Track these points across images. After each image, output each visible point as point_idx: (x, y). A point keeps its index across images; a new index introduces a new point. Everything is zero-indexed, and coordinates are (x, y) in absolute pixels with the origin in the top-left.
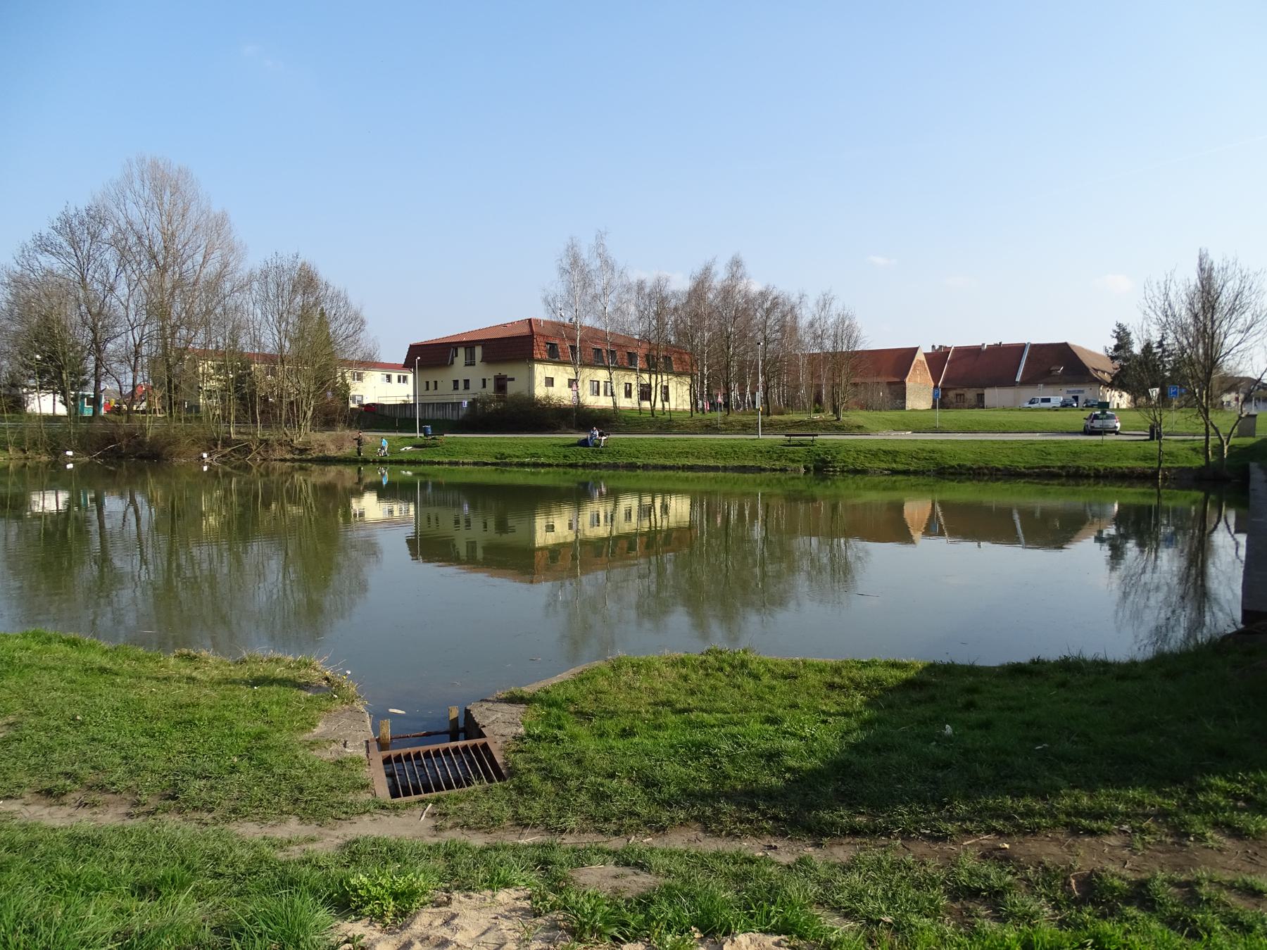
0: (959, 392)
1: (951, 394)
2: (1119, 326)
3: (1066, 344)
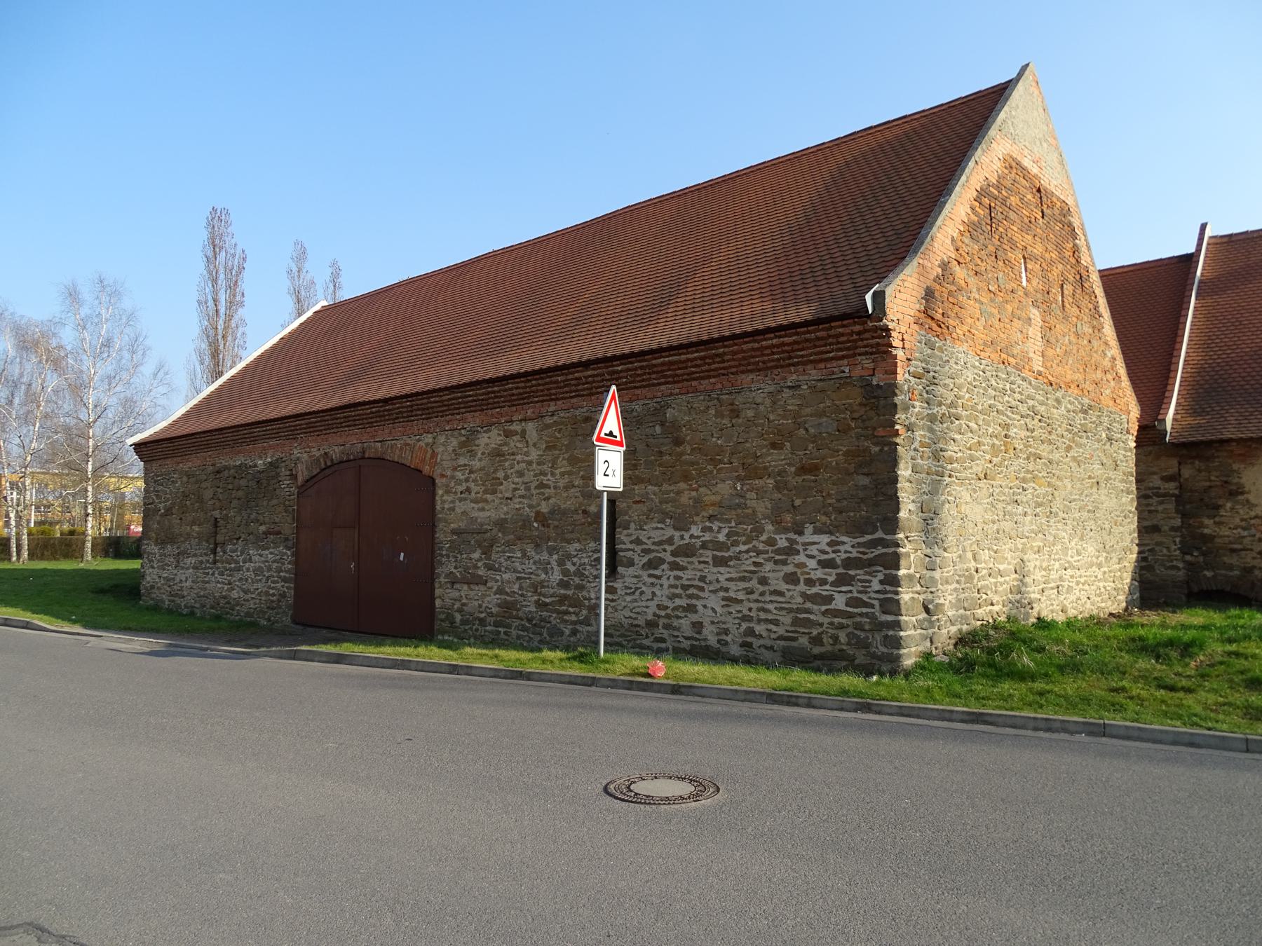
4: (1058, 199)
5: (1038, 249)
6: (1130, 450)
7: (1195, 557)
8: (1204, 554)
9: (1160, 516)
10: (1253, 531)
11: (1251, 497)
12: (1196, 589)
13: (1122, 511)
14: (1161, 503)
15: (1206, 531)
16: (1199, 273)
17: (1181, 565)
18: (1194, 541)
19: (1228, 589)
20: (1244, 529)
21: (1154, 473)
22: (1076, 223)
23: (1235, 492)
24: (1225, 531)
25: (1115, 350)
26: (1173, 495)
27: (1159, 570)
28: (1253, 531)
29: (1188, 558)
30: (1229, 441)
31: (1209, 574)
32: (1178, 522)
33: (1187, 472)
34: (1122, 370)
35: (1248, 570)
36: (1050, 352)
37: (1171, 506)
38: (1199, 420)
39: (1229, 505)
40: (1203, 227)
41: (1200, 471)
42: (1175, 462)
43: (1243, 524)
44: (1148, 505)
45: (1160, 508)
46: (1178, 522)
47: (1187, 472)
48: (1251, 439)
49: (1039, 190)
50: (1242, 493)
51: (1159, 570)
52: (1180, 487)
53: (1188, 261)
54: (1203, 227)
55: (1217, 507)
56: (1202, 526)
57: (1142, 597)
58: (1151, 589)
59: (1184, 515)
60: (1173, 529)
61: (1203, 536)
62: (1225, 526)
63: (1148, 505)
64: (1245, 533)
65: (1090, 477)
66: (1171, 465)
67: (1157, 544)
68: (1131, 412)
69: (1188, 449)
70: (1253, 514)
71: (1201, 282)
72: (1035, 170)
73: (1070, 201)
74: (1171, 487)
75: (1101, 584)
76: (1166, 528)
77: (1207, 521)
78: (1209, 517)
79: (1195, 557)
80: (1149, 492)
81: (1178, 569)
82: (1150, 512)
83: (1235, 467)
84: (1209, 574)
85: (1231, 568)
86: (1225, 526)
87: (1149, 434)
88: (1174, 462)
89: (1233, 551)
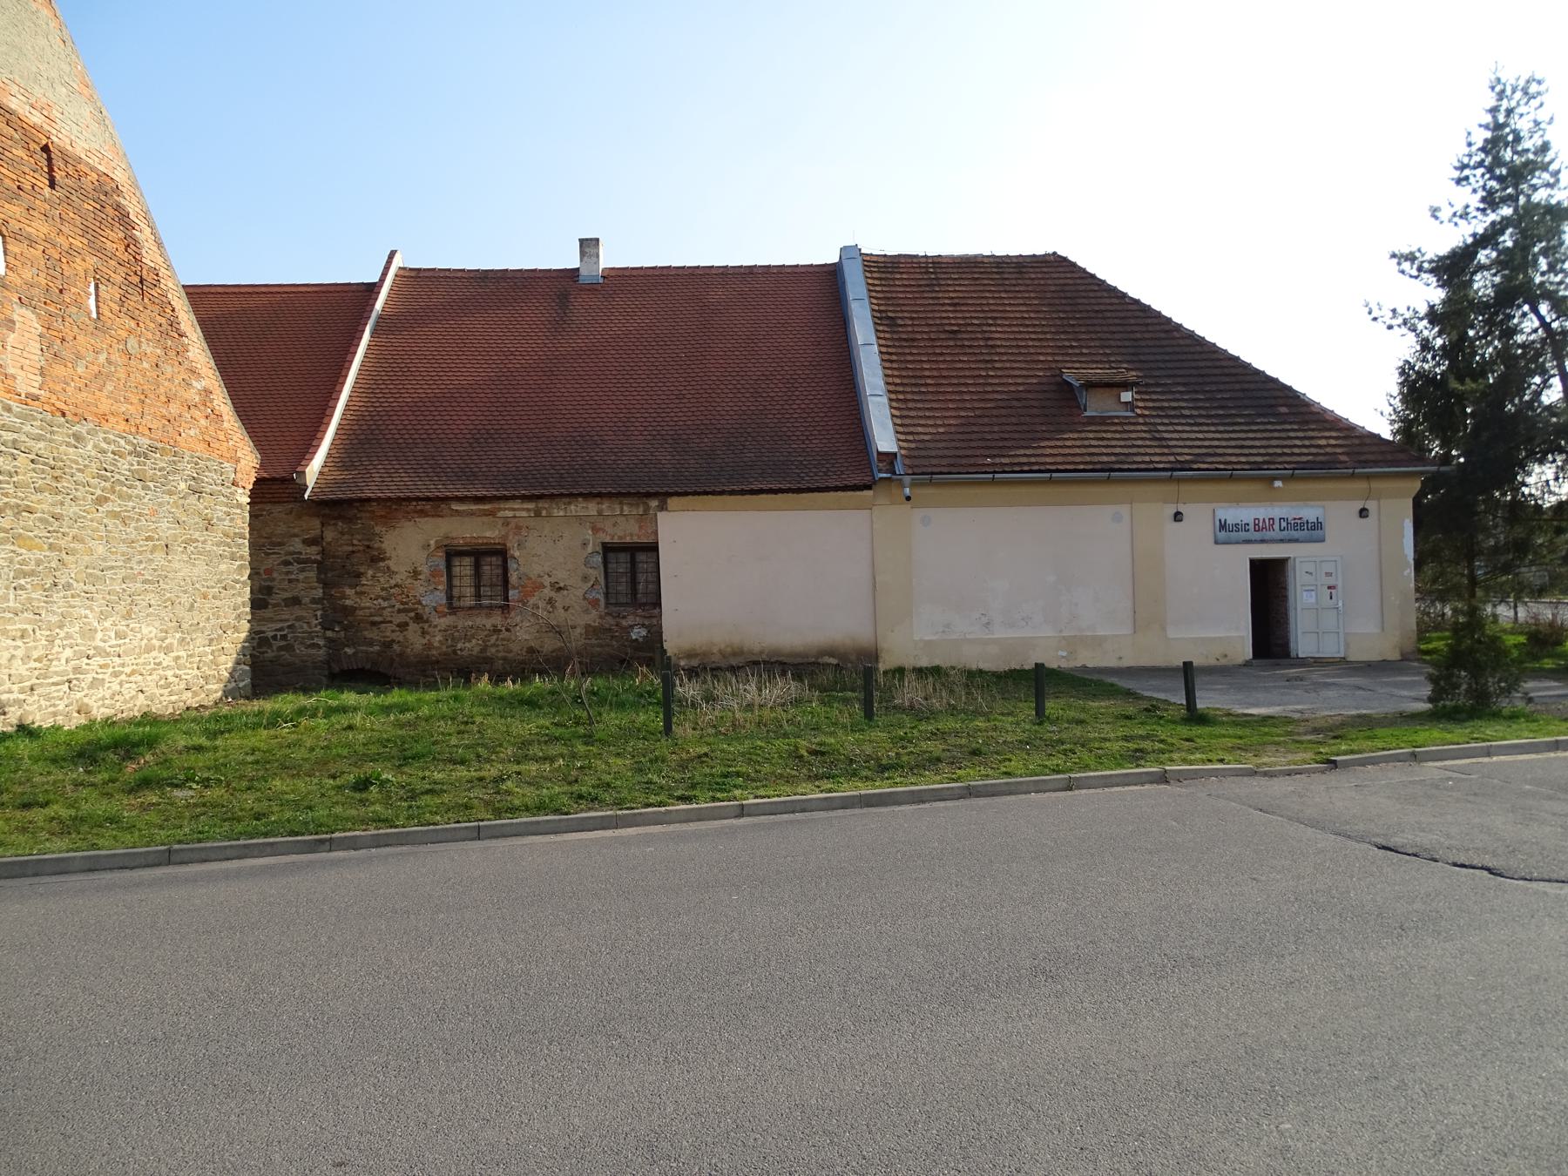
0: (470, 528)
1: (410, 547)
2: (1506, 163)
3: (1055, 266)
4: (93, 169)
5: (38, 228)
6: (239, 506)
7: (336, 633)
8: (345, 629)
9: (301, 586)
10: (393, 602)
11: (391, 563)
12: (336, 670)
13: (220, 581)
14: (303, 570)
15: (348, 602)
16: (379, 305)
17: (321, 643)
18: (337, 615)
19: (368, 667)
20: (384, 599)
21: (296, 535)
22: (133, 210)
23: (376, 558)
24: (366, 603)
25: (209, 377)
26: (315, 561)
27: (300, 650)
28: (393, 602)
29: (329, 634)
30: (369, 500)
31: (349, 651)
32: (319, 593)
33: (330, 535)
34: (222, 403)
35: (388, 645)
36: (59, 370)
37: (312, 574)
38: (346, 475)
39: (370, 572)
40: (392, 254)
41: (342, 533)
42: (316, 523)
43: (383, 594)
44: (288, 573)
45: (301, 577)
46: (319, 593)
47: (330, 535)
48: (390, 499)
49: (45, 149)
50: (383, 560)
51: (300, 650)
52: (323, 552)
53: (371, 289)
54: (392, 254)
55: (359, 575)
56: (344, 597)
57: (254, 686)
58: (265, 669)
59: (326, 585)
60: (314, 601)
61: (345, 608)
62: (365, 597)
63: (288, 573)
64: (385, 604)
65: (148, 539)
66: (314, 526)
67: (298, 619)
68: (247, 463)
69: (331, 507)
70: (393, 582)
71: (380, 317)
72: (36, 118)
73: (119, 176)
74: (312, 552)
75: (169, 673)
76: (307, 600)
77: (349, 591)
78: (351, 587)
79: (336, 633)
80: (290, 558)
81: (318, 646)
82: (290, 581)
83: (377, 529)
84: (349, 651)
85: (371, 643)
86: (365, 597)
87: (273, 491)
88: (316, 523)
89: (374, 624)
